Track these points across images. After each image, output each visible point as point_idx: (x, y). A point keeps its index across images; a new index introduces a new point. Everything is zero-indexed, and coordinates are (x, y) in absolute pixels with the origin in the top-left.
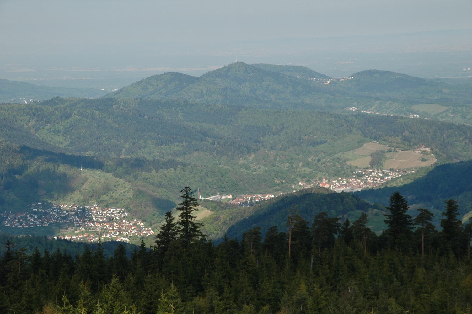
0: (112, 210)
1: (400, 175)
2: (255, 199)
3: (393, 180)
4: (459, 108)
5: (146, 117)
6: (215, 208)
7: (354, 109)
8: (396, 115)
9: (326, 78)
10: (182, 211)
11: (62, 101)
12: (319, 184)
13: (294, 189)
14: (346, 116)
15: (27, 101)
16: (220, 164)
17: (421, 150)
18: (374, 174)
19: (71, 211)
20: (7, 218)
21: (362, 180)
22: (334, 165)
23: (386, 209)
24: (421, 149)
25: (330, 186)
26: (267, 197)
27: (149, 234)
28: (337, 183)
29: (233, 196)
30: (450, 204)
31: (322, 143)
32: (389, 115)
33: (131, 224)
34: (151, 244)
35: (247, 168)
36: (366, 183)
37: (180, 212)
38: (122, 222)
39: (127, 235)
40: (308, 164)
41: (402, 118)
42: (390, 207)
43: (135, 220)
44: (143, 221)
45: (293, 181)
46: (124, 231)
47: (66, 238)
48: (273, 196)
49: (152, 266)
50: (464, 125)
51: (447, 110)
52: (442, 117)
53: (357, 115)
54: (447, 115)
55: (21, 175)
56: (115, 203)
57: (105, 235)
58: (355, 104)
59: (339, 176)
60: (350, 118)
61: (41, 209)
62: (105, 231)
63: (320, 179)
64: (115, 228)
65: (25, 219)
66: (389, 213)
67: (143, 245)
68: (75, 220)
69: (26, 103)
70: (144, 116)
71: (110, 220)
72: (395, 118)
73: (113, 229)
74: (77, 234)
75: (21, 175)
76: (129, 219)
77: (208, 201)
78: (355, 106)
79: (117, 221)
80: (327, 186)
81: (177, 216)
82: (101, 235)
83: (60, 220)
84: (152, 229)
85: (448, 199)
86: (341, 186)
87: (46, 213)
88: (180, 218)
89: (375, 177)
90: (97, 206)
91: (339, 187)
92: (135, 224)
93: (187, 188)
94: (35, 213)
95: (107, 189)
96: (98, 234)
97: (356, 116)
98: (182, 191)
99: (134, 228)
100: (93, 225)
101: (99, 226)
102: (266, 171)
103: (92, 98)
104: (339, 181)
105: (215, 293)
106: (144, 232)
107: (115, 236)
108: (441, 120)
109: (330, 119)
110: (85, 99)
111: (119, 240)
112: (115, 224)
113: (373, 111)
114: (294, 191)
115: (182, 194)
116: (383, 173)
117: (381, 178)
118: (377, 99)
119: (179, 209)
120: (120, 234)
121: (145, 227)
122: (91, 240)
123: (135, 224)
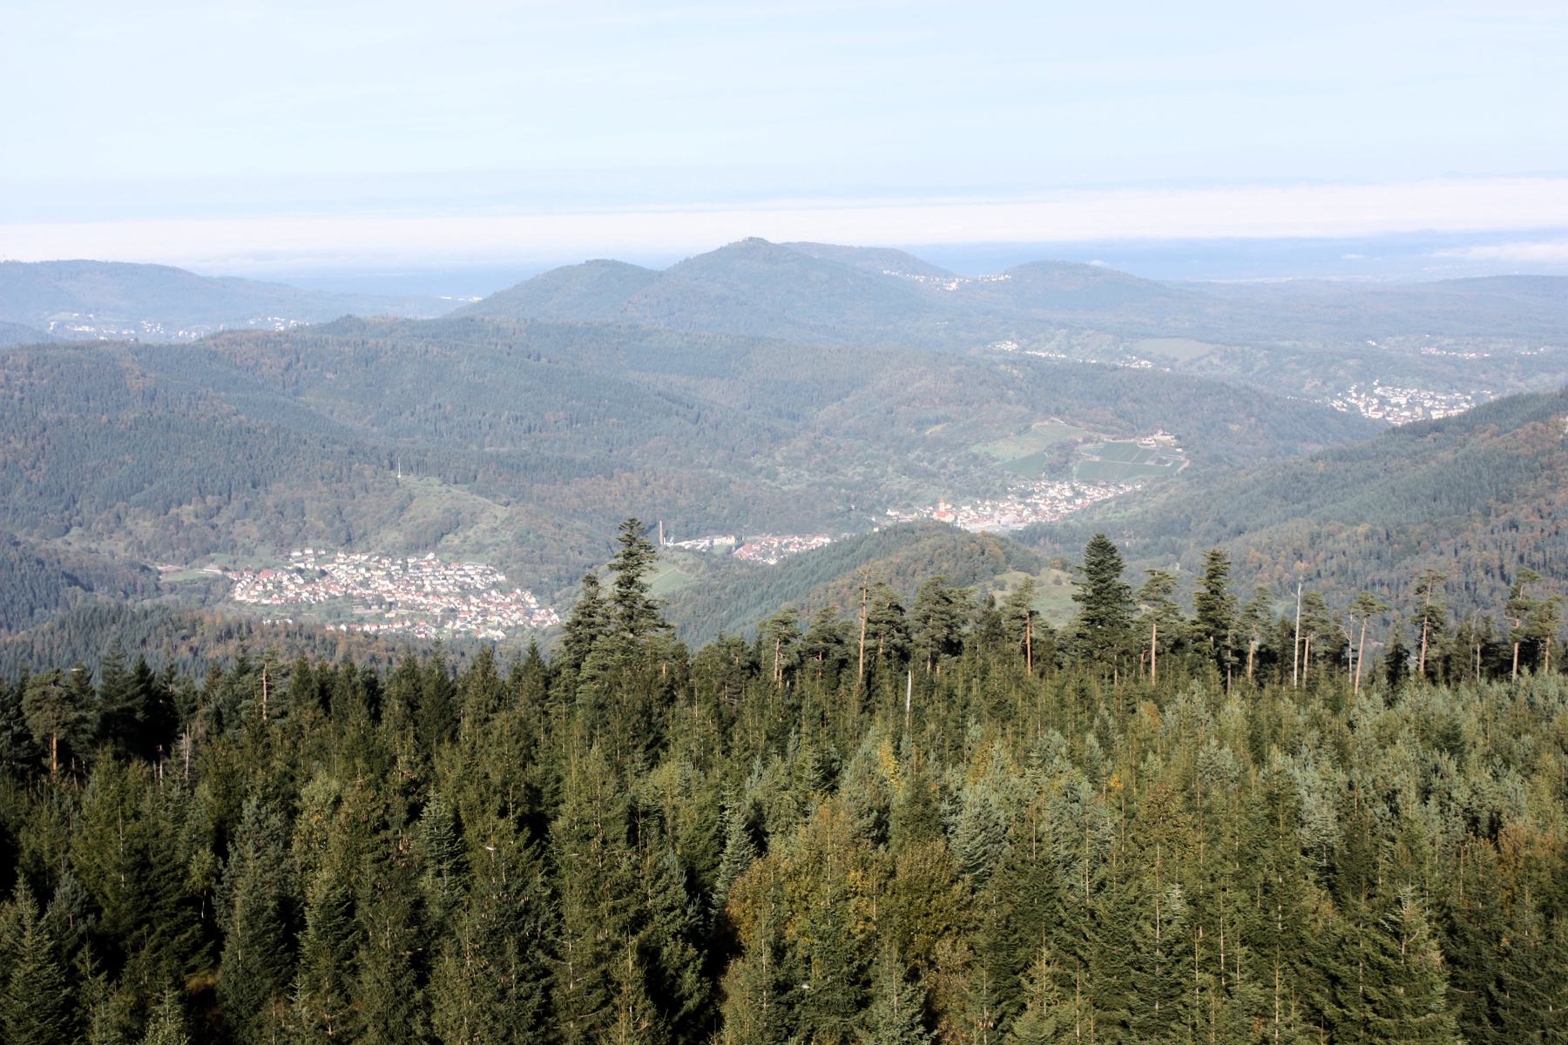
0: (466, 568)
1: (1110, 495)
2: (787, 546)
3: (1097, 505)
5: (544, 360)
7: (1010, 346)
8: (1104, 361)
9: (949, 275)
10: (622, 573)
11: (362, 325)
12: (931, 513)
14: (994, 363)
15: (283, 324)
16: (710, 467)
18: (1052, 492)
19: (378, 568)
20: (239, 581)
21: (1028, 505)
22: (965, 473)
24: (1156, 437)
25: (956, 518)
26: (814, 541)
27: (549, 623)
28: (972, 512)
29: (738, 539)
30: (1215, 558)
32: (1088, 361)
33: (508, 600)
34: (553, 649)
37: (617, 575)
38: (489, 594)
39: (500, 623)
40: (908, 470)
41: (1115, 368)
42: (1084, 566)
43: (518, 591)
44: (535, 592)
45: (877, 507)
46: (492, 614)
47: (367, 628)
48: (828, 540)
49: (516, 839)
50: (1246, 387)
51: (1212, 353)
52: (1201, 368)
53: (1017, 361)
54: (1210, 363)
56: (478, 550)
57: (451, 623)
58: (1013, 334)
59: (977, 494)
60: (1002, 367)
62: (452, 613)
63: (935, 503)
64: (472, 608)
65: (279, 586)
66: (1084, 577)
67: (533, 650)
68: (385, 589)
69: (282, 328)
70: (539, 358)
71: (465, 592)
72: (1100, 367)
73: (470, 611)
74: (390, 621)
76: (503, 589)
78: (1012, 340)
79: (478, 593)
80: (949, 519)
81: (609, 586)
82: (443, 623)
83: (354, 589)
84: (556, 612)
85: (1210, 549)
86: (982, 517)
87: (323, 573)
88: (616, 586)
89: (1055, 498)
90: (434, 560)
91: (975, 521)
92: (518, 601)
93: (632, 520)
94: (300, 571)
95: (453, 523)
96: (436, 621)
97: (1014, 363)
99: (518, 609)
100: (425, 601)
101: (438, 602)
102: (814, 484)
103: (425, 318)
104: (975, 507)
105: (812, 982)
106: (539, 618)
107: (474, 627)
109: (957, 368)
110: (409, 321)
111: (482, 636)
112: (473, 600)
113: (1052, 352)
114: (876, 530)
115: (622, 535)
116: (1073, 488)
117: (1069, 500)
118: (1062, 325)
119: (612, 567)
120: (485, 622)
121: (540, 608)
122: (420, 633)
123: (518, 601)
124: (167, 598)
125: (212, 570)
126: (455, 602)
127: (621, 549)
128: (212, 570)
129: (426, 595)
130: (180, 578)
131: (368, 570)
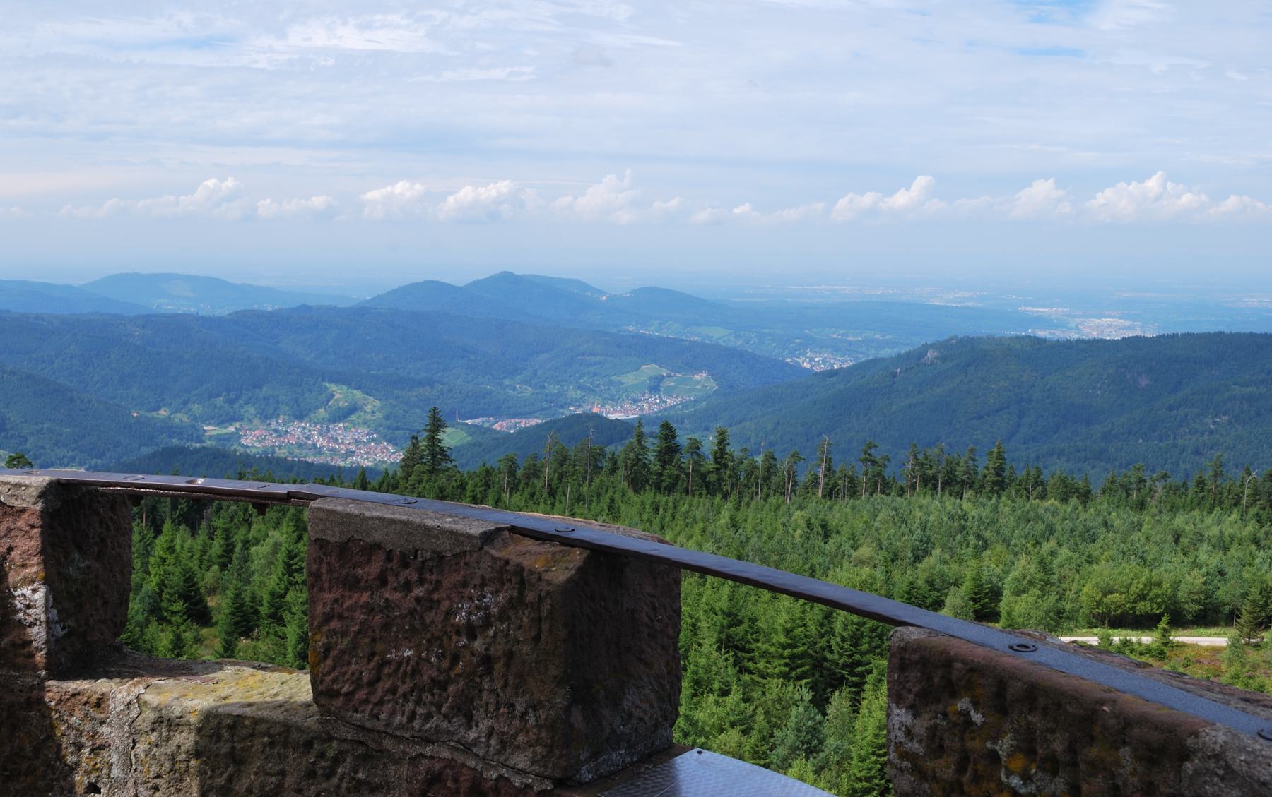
4: (742, 333)
6: (474, 433)
7: (631, 328)
13: (562, 414)
17: (500, 384)
23: (860, 463)
31: (421, 384)
35: (514, 389)
36: (642, 409)
41: (683, 340)
52: (724, 342)
55: (500, 775)
61: (341, 699)
62: (350, 453)
71: (357, 442)
72: (675, 339)
75: (500, 775)
77: (467, 424)
79: (365, 444)
98: (430, 411)
108: (724, 345)
124: (208, 443)
125: (231, 429)
126: (353, 448)
127: (428, 421)
128: (231, 429)
129: (339, 444)
130: (215, 433)
131: (310, 431)
